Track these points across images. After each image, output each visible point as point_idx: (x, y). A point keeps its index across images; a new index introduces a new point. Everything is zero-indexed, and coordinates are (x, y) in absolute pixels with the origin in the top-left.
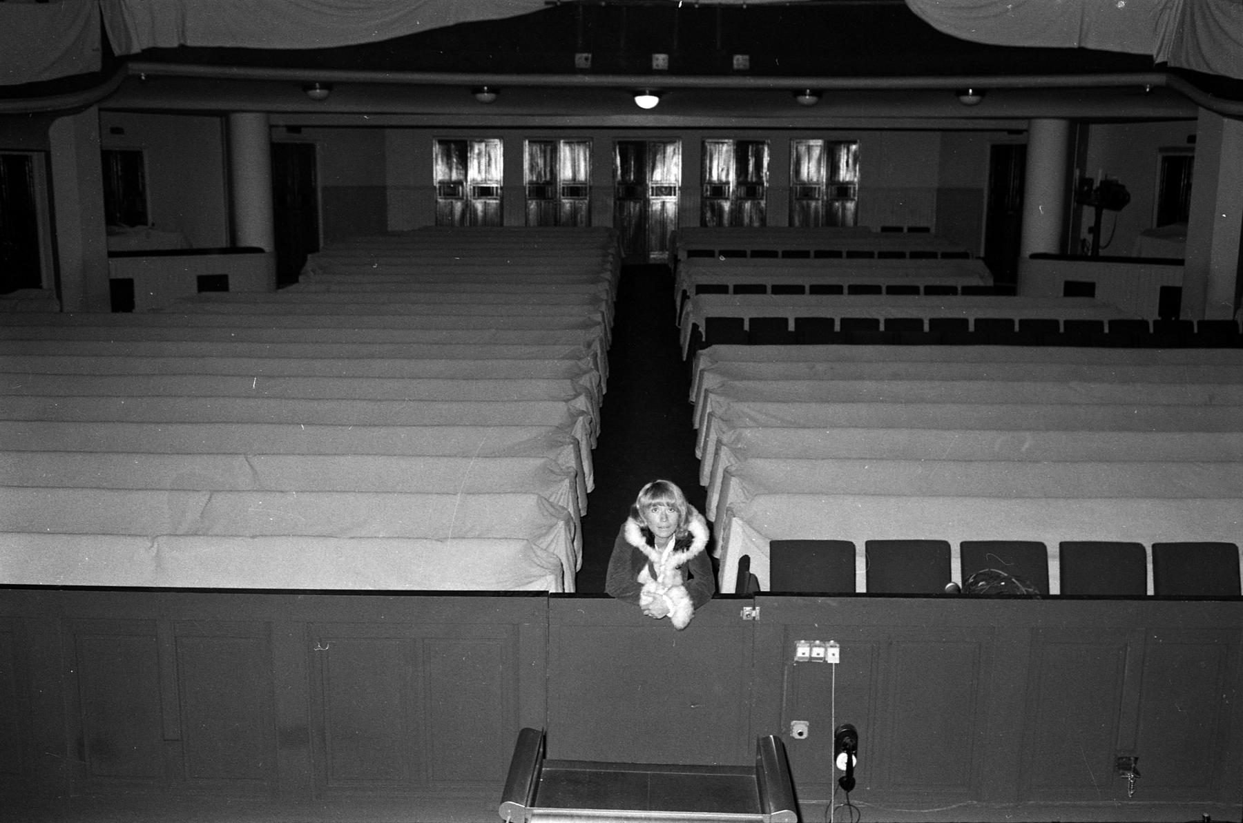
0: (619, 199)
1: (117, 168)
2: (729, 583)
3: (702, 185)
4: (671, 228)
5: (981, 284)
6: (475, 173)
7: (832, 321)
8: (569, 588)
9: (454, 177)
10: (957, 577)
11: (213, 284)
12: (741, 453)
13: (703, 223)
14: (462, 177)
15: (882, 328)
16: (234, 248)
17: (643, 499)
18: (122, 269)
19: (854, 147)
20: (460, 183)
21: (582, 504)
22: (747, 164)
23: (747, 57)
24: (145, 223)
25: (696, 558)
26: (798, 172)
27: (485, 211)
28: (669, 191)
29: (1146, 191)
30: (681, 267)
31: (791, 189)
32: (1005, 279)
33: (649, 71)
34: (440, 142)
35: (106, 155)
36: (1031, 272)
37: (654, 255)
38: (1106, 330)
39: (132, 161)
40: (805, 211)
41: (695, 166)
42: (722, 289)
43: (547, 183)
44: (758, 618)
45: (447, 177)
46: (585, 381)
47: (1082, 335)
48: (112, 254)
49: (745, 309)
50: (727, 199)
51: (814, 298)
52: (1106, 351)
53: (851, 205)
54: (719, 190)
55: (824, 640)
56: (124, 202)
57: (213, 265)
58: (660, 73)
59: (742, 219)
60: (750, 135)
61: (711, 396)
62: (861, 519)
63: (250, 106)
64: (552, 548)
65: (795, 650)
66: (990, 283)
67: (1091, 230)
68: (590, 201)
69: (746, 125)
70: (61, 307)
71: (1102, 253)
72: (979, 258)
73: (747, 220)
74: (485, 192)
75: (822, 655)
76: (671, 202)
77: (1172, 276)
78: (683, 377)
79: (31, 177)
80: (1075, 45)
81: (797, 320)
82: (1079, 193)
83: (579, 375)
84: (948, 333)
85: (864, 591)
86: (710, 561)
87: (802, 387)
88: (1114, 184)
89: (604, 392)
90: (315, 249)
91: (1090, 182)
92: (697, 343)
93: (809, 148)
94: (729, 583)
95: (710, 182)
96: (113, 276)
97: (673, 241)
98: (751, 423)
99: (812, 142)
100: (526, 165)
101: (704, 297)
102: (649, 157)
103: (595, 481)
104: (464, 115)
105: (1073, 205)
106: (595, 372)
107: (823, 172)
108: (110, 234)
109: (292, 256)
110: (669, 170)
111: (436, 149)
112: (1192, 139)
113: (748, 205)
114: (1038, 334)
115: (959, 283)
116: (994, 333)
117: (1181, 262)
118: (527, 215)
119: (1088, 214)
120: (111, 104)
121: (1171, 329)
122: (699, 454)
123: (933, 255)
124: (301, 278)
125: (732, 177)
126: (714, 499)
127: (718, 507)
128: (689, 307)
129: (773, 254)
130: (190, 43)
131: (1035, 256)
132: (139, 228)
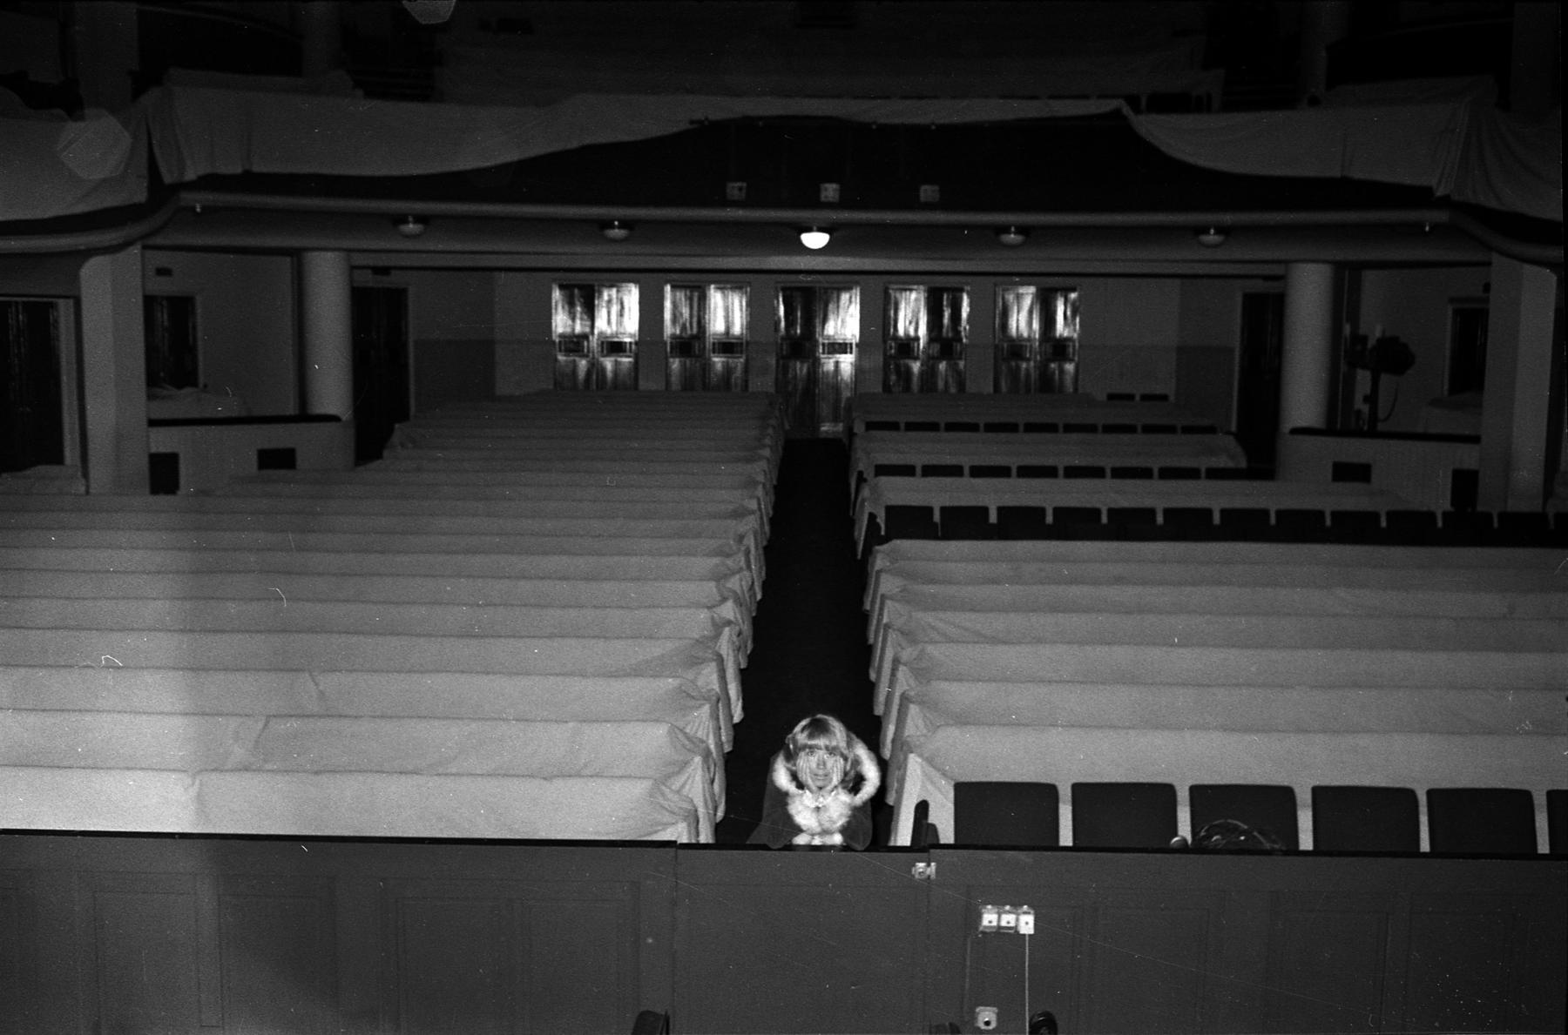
0: (783, 357)
1: (163, 317)
2: (903, 835)
3: (885, 342)
4: (846, 394)
5: (1231, 464)
6: (603, 324)
7: (1042, 511)
8: (705, 837)
9: (578, 329)
10: (1185, 830)
11: (277, 460)
12: (923, 673)
13: (887, 388)
14: (587, 330)
15: (1104, 519)
16: (304, 416)
17: (800, 734)
18: (163, 440)
19: (1073, 296)
20: (585, 337)
21: (725, 736)
22: (941, 316)
23: (936, 188)
24: (194, 384)
25: (865, 804)
26: (1005, 325)
27: (616, 372)
28: (843, 348)
29: (1435, 345)
30: (858, 443)
31: (996, 347)
32: (1261, 458)
33: (817, 204)
34: (562, 287)
35: (149, 302)
36: (1293, 451)
37: (826, 428)
38: (1384, 524)
39: (181, 307)
40: (1014, 374)
41: (878, 317)
42: (907, 471)
43: (693, 337)
44: (933, 877)
45: (568, 330)
46: (734, 583)
47: (1354, 529)
48: (153, 423)
49: (936, 495)
50: (916, 358)
51: (1024, 483)
52: (1383, 551)
53: (1070, 367)
54: (907, 346)
55: (1016, 905)
56: (171, 354)
57: (277, 437)
58: (830, 206)
59: (935, 384)
60: (940, 281)
61: (888, 603)
62: (1066, 750)
63: (323, 243)
64: (685, 791)
65: (979, 917)
66: (1243, 464)
67: (1366, 399)
68: (747, 361)
69: (949, 269)
70: (88, 487)
71: (1381, 427)
72: (1229, 433)
73: (941, 385)
74: (614, 347)
75: (1012, 924)
76: (847, 362)
77: (1467, 457)
78: (857, 577)
79: (56, 328)
80: (1338, 175)
81: (1000, 510)
82: (1348, 352)
83: (726, 577)
84: (1187, 526)
85: (1070, 844)
86: (879, 812)
87: (1007, 592)
88: (1394, 340)
89: (759, 597)
90: (404, 416)
91: (1365, 339)
92: (875, 537)
93: (1019, 297)
94: (903, 835)
95: (896, 338)
96: (154, 450)
97: (849, 409)
98: (937, 638)
99: (1022, 290)
100: (668, 315)
101: (883, 479)
102: (819, 307)
103: (744, 708)
104: (588, 255)
105: (1343, 368)
106: (746, 573)
107: (1036, 325)
108: (151, 397)
109: (377, 422)
110: (845, 321)
111: (557, 294)
112: (1487, 288)
113: (942, 366)
114: (1299, 527)
115: (1204, 463)
116: (1244, 526)
117: (1475, 440)
118: (668, 376)
119: (1363, 378)
120: (159, 240)
121: (1468, 522)
122: (873, 676)
123: (1170, 429)
124: (386, 453)
125: (923, 331)
126: (890, 731)
127: (893, 741)
128: (866, 492)
129: (973, 428)
130: (257, 168)
131: (1297, 431)
132: (187, 390)
